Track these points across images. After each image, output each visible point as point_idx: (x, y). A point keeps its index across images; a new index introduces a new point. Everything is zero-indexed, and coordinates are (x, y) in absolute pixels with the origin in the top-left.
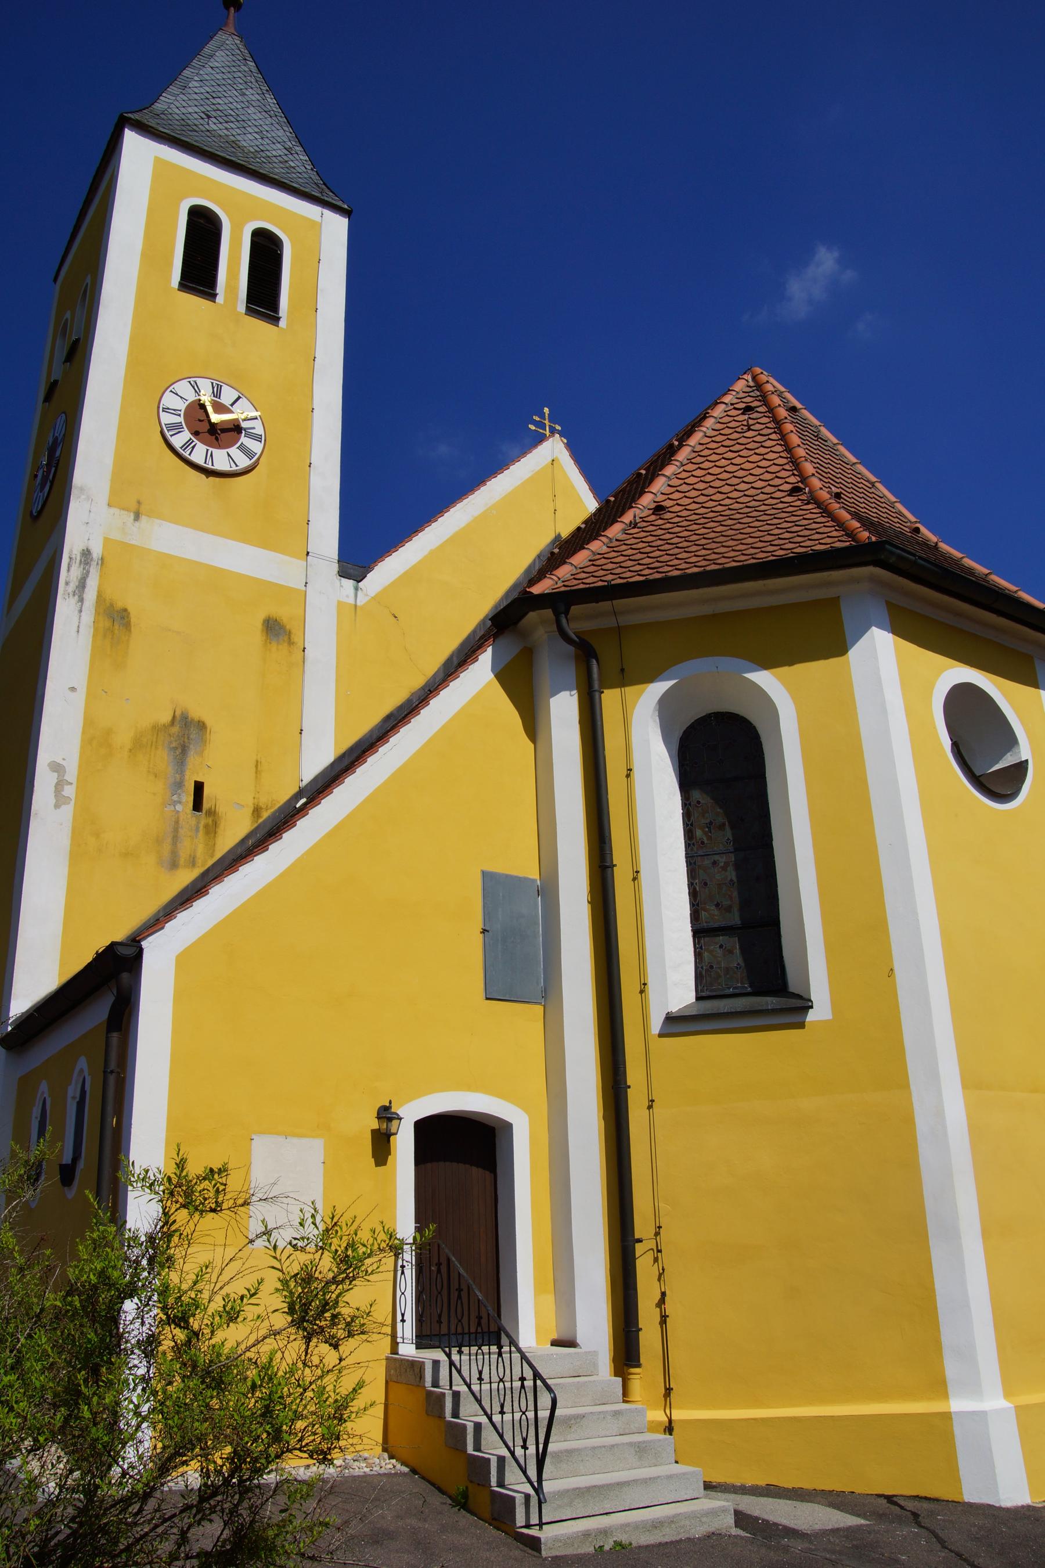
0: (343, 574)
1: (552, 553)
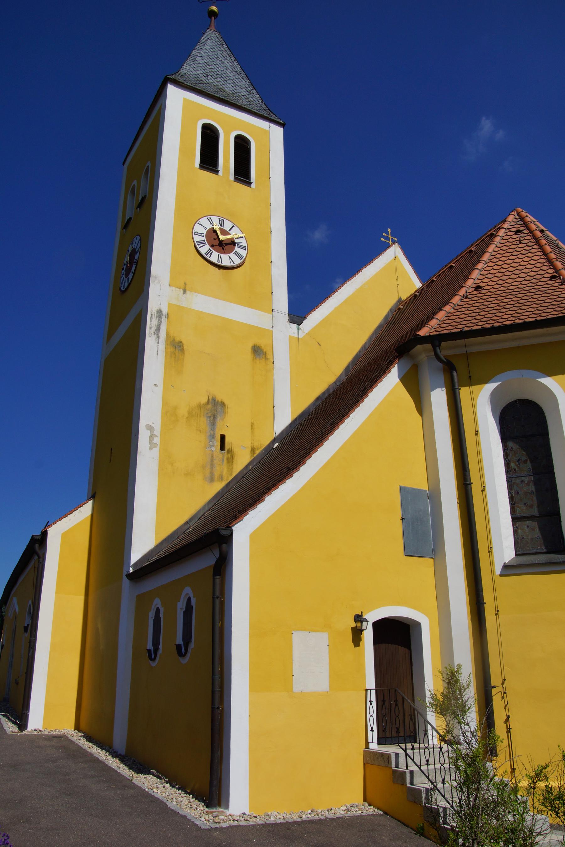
0: (291, 321)
1: (399, 309)
